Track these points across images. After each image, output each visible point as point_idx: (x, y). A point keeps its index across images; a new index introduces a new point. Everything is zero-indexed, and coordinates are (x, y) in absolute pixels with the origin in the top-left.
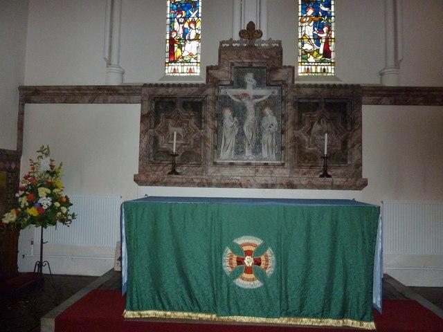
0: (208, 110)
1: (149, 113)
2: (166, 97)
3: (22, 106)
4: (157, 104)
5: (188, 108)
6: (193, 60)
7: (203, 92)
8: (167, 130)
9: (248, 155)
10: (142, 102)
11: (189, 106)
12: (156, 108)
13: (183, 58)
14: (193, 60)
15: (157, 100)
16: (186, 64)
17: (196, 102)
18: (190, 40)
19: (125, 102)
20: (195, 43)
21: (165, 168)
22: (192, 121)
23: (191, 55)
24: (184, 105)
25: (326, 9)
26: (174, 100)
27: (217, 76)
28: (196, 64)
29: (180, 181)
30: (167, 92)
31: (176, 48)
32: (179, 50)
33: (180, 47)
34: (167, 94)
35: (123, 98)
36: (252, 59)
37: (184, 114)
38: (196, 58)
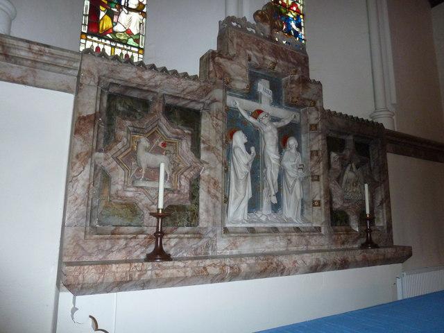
0: (209, 128)
1: (96, 116)
2: (137, 88)
3: (99, 330)
4: (112, 97)
5: (175, 118)
6: (131, 41)
7: (207, 93)
8: (132, 155)
9: (264, 216)
10: (78, 89)
11: (177, 114)
12: (109, 108)
13: (114, 33)
14: (131, 41)
15: (114, 90)
16: (119, 45)
17: (189, 110)
18: (130, 10)
19: (22, 81)
20: (136, 17)
21: (133, 243)
22: (185, 146)
23: (128, 32)
24: (169, 111)
25: (297, 30)
26: (150, 98)
27: (229, 71)
28: (136, 50)
29: (181, 274)
30: (140, 77)
31: (102, 14)
32: (108, 18)
33: (110, 14)
34: (139, 81)
35: (16, 71)
36: (276, 58)
37: (166, 129)
38: (137, 41)
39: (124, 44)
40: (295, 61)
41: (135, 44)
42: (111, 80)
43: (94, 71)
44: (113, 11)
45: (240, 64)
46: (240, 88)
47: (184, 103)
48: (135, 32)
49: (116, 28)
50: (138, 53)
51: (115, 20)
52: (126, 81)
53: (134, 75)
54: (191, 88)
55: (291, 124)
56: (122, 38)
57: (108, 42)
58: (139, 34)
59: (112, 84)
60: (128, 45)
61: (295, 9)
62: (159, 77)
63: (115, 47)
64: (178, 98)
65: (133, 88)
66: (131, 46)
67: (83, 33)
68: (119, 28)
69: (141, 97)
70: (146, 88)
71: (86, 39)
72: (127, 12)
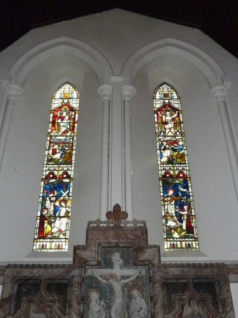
1: (9, 298)
2: (31, 279)
4: (20, 286)
14: (61, 236)
16: (54, 240)
23: (60, 231)
24: (49, 288)
25: (185, 190)
28: (64, 240)
30: (32, 273)
31: (46, 225)
32: (49, 226)
33: (50, 223)
34: (31, 275)
36: (118, 239)
38: (64, 235)
39: (57, 239)
40: (133, 237)
41: (64, 237)
42: (18, 278)
43: (10, 275)
44: (51, 221)
45: (91, 251)
46: (74, 270)
47: (56, 281)
48: (63, 230)
49: (53, 231)
50: (65, 242)
51: (53, 226)
52: (25, 277)
53: (29, 273)
54: (59, 273)
55: (137, 278)
56: (56, 235)
57: (48, 240)
58: (66, 230)
59: (18, 279)
60: (59, 239)
61: (181, 175)
62: (42, 271)
63: (52, 242)
64: (53, 279)
65: (29, 279)
66: (61, 239)
67: (35, 239)
68: (54, 230)
69: (34, 282)
70: (34, 278)
71: (37, 242)
72: (59, 219)
